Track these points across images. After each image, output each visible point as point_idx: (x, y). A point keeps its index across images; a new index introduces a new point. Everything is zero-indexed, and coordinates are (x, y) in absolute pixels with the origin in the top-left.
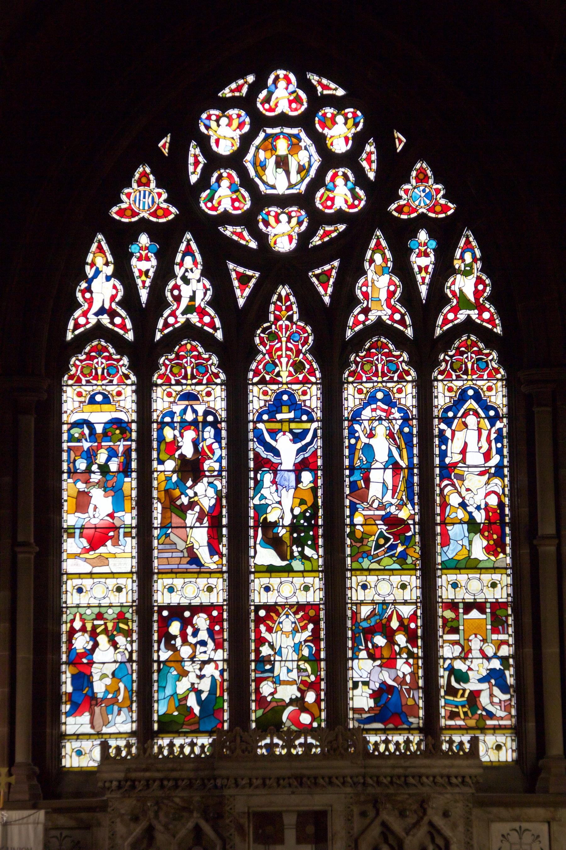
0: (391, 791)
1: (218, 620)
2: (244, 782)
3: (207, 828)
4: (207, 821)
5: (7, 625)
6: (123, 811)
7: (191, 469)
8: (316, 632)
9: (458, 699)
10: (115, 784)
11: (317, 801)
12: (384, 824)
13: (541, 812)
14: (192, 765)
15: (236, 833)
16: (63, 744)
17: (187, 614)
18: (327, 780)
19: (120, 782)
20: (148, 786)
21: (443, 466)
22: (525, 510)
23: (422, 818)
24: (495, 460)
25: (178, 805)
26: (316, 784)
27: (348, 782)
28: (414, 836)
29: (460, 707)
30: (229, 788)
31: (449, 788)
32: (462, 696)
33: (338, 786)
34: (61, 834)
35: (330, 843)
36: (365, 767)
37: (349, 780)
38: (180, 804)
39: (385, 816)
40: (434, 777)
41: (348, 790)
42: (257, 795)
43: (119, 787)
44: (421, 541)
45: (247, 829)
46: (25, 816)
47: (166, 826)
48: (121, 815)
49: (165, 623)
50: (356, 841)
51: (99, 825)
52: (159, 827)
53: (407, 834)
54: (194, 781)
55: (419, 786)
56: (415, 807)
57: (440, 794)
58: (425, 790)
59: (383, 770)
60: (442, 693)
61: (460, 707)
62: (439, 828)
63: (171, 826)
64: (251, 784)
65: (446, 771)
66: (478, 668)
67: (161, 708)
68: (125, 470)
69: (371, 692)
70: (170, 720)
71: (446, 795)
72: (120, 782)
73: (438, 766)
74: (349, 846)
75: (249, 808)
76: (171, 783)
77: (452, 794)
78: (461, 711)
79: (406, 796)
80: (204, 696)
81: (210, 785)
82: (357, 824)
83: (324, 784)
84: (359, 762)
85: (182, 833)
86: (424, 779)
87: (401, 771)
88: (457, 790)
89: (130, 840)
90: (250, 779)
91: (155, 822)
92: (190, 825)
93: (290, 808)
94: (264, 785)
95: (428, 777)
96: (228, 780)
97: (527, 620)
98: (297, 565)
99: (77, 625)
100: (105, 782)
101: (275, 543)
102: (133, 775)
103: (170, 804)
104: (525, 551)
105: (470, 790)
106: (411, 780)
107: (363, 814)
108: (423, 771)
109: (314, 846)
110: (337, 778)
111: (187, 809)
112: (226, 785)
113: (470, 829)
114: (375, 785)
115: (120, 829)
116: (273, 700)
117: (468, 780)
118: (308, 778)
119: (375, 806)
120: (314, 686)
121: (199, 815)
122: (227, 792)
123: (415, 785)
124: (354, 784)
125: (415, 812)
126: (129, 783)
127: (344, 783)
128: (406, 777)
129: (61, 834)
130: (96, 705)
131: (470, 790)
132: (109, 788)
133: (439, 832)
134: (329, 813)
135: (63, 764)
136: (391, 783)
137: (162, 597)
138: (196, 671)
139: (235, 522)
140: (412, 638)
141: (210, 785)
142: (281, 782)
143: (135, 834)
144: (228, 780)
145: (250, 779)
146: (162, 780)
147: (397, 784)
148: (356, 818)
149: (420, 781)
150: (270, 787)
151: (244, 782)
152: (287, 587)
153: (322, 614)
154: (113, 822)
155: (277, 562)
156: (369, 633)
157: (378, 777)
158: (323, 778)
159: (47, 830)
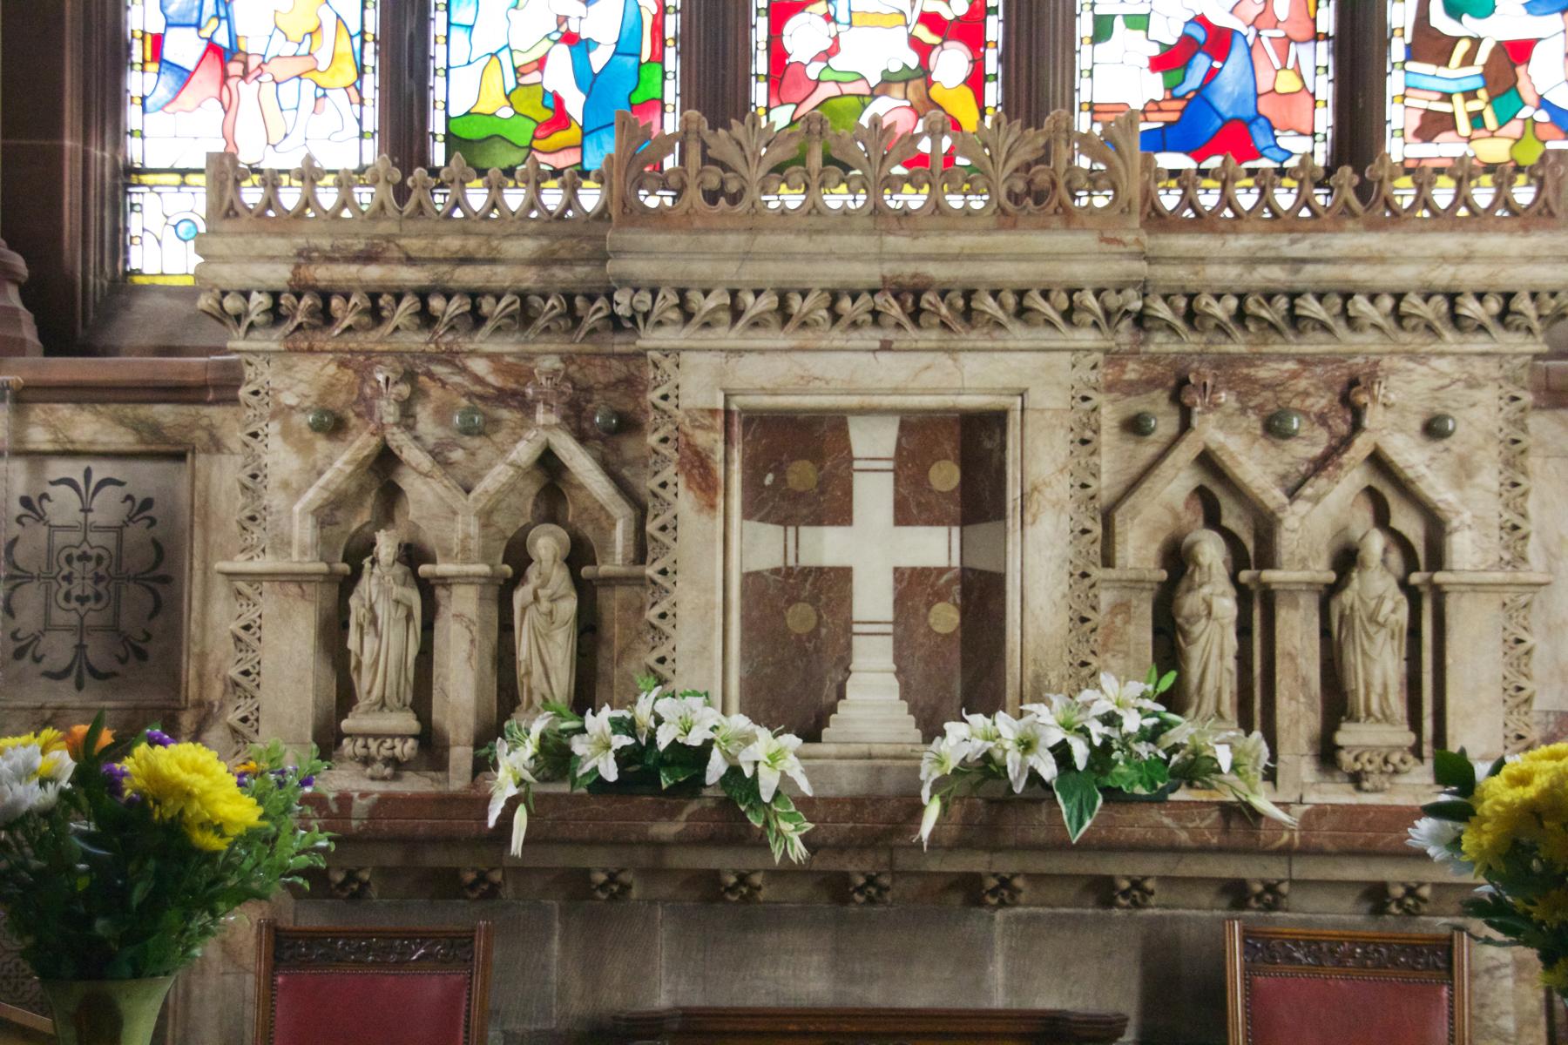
0: (1238, 345)
2: (711, 303)
3: (581, 464)
4: (582, 438)
6: (289, 399)
9: (1454, 69)
10: (259, 301)
11: (966, 376)
12: (1207, 461)
14: (527, 247)
15: (681, 480)
16: (135, 199)
18: (1010, 300)
19: (275, 295)
20: (376, 315)
23: (1345, 442)
25: (478, 380)
26: (968, 315)
27: (1089, 310)
28: (1316, 499)
29: (1458, 99)
30: (660, 323)
31: (1449, 335)
32: (1468, 59)
33: (1049, 323)
34: (88, 474)
35: (1013, 521)
36: (1151, 260)
37: (1090, 300)
38: (491, 379)
39: (1225, 432)
40: (1399, 297)
41: (1086, 337)
42: (762, 351)
43: (276, 315)
45: (720, 472)
46: (568, 607)
47: (438, 454)
48: (282, 412)
50: (1107, 519)
51: (216, 445)
52: (412, 454)
53: (1293, 494)
54: (536, 301)
55: (1340, 328)
56: (1319, 402)
57: (1412, 356)
58: (1367, 342)
59: (1213, 272)
60: (1397, 50)
61: (1458, 99)
62: (1410, 474)
63: (457, 455)
64: (736, 312)
65: (1443, 276)
69: (1155, 51)
70: (483, 134)
71: (1436, 363)
72: (275, 295)
74: (1085, 531)
75: (727, 397)
76: (457, 306)
77: (1460, 357)
78: (1460, 109)
79: (1291, 365)
80: (598, 60)
81: (593, 316)
82: (1114, 460)
83: (1000, 315)
84: (1129, 238)
85: (496, 477)
86: (1360, 304)
87: (1276, 275)
88: (1479, 343)
89: (313, 495)
90: (734, 294)
91: (399, 440)
92: (525, 451)
93: (875, 401)
94: (783, 313)
95: (1373, 298)
96: (654, 293)
100: (224, 293)
102: (323, 274)
103: (457, 379)
106: (1311, 307)
107: (1135, 426)
108: (1359, 273)
109: (956, 531)
110: (1045, 294)
112: (646, 315)
113: (1521, 479)
114: (1179, 323)
115: (280, 458)
116: (827, 75)
117: (1523, 304)
118: (943, 294)
119: (1176, 398)
121: (554, 419)
123: (1324, 327)
124: (1108, 314)
125: (1322, 419)
126: (307, 301)
127: (1068, 315)
128: (1294, 295)
129: (88, 474)
130: (245, 76)
132: (238, 318)
133: (1405, 488)
134: (1014, 419)
135: (134, 264)
136: (1241, 316)
141: (593, 316)
142: (845, 304)
143: (328, 475)
144: (654, 293)
145: (734, 294)
146: (423, 295)
147: (1259, 319)
148: (1109, 436)
149: (1345, 310)
150: (804, 325)
151: (711, 303)
154: (255, 435)
157: (1191, 297)
158: (995, 294)
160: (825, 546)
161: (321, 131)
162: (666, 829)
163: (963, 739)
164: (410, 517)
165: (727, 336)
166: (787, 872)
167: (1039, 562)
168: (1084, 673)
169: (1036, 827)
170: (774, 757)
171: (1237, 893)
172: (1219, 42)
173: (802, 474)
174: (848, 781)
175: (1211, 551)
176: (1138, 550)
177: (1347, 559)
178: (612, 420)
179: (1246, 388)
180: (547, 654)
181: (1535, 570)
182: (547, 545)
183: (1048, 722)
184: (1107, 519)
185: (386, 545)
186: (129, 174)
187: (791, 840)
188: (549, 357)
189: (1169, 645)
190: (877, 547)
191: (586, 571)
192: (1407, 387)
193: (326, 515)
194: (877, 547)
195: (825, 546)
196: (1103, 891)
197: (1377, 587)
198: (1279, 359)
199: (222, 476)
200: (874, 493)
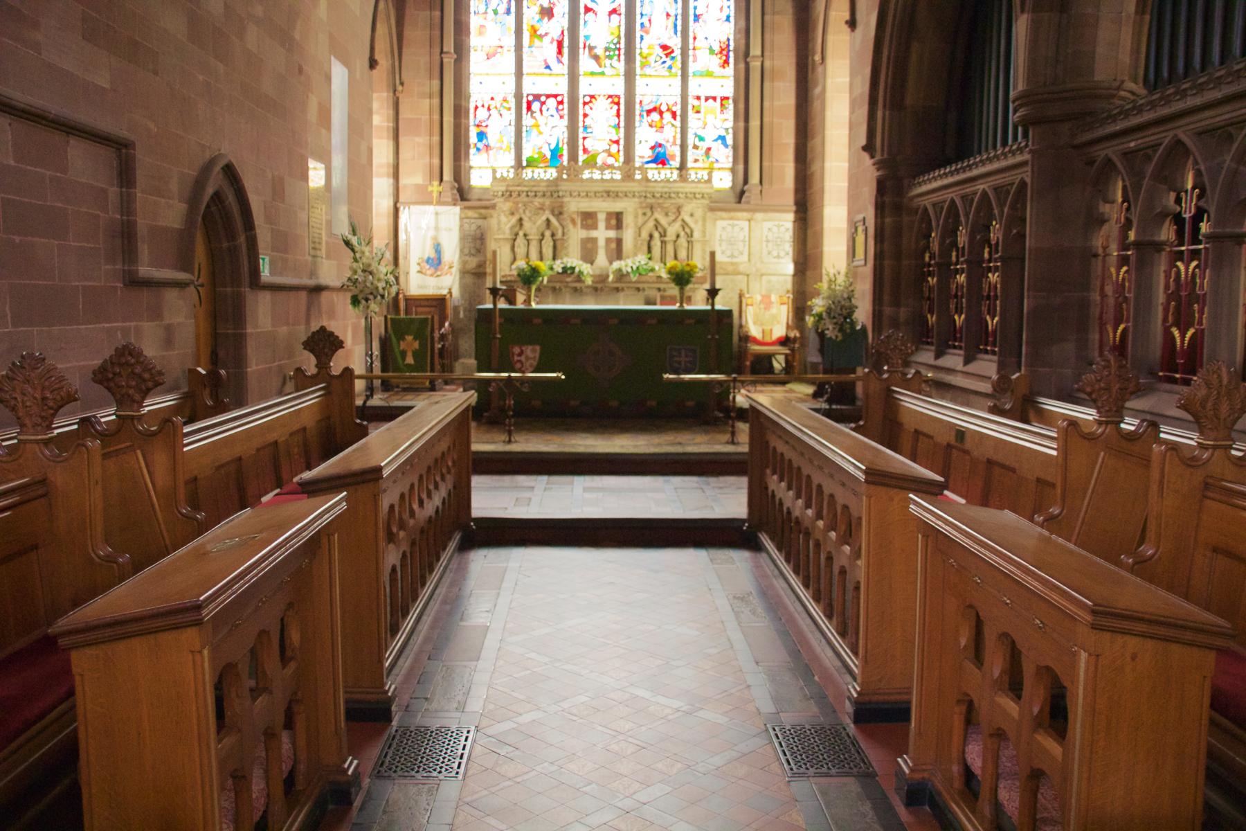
1: (561, 103)
3: (553, 220)
5: (73, 141)
7: (548, 13)
8: (618, 111)
11: (616, 206)
13: (745, 215)
17: (543, 99)
21: (695, 16)
22: (743, 41)
24: (726, 12)
39: (658, 215)
44: (680, 56)
46: (552, 244)
49: (529, 104)
50: (640, 229)
53: (670, 224)
58: (680, 201)
66: (710, 134)
67: (527, 153)
68: (508, 12)
73: (687, 188)
82: (641, 220)
89: (509, 225)
92: (544, 218)
97: (742, 106)
98: (608, 71)
99: (479, 105)
101: (596, 58)
104: (742, 66)
105: (706, 202)
107: (644, 214)
111: (542, 208)
115: (504, 219)
120: (617, 142)
122: (566, 200)
131: (706, 202)
137: (529, 88)
138: (547, 131)
139: (570, 46)
140: (674, 115)
152: (602, 82)
153: (622, 101)
155: (596, 68)
156: (649, 112)
159: (461, 219)
160: (594, 234)
161: (504, 161)
162: (569, 279)
163: (616, 265)
164: (767, 320)
165: (578, 199)
166: (588, 287)
167: (628, 236)
168: (635, 255)
169: (627, 279)
170: (586, 268)
171: (659, 290)
172: (660, 145)
173: (590, 222)
174: (598, 272)
175: (656, 235)
176: (645, 235)
177: (678, 236)
178: (559, 214)
179: (662, 208)
180: (548, 251)
181: (707, 238)
182: (548, 233)
183: (629, 262)
184: (640, 229)
185: (521, 233)
186: (471, 168)
187: (589, 281)
188: (548, 202)
189: (649, 251)
190: (602, 234)
191: (778, 364)
192: (687, 209)
193: (511, 228)
194: (602, 234)
195: (594, 234)
196: (638, 289)
197: (683, 241)
198: (667, 204)
199: (493, 222)
200: (602, 225)
